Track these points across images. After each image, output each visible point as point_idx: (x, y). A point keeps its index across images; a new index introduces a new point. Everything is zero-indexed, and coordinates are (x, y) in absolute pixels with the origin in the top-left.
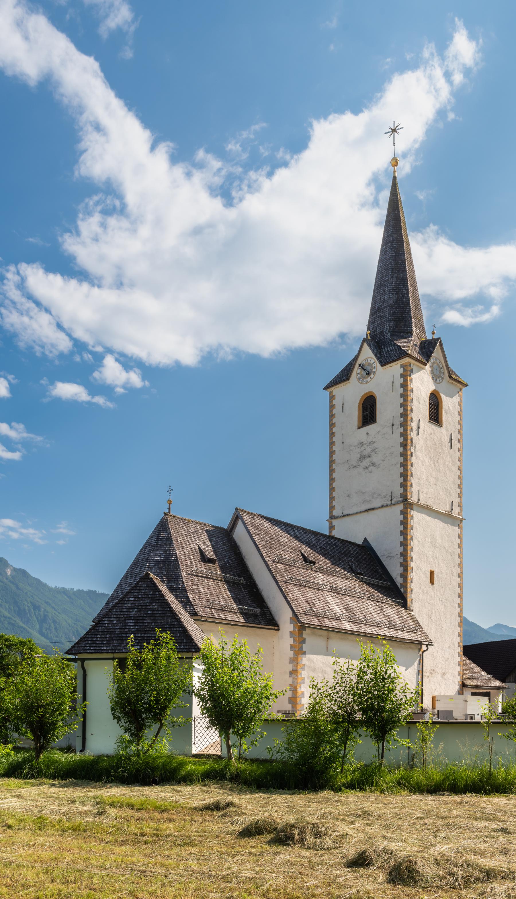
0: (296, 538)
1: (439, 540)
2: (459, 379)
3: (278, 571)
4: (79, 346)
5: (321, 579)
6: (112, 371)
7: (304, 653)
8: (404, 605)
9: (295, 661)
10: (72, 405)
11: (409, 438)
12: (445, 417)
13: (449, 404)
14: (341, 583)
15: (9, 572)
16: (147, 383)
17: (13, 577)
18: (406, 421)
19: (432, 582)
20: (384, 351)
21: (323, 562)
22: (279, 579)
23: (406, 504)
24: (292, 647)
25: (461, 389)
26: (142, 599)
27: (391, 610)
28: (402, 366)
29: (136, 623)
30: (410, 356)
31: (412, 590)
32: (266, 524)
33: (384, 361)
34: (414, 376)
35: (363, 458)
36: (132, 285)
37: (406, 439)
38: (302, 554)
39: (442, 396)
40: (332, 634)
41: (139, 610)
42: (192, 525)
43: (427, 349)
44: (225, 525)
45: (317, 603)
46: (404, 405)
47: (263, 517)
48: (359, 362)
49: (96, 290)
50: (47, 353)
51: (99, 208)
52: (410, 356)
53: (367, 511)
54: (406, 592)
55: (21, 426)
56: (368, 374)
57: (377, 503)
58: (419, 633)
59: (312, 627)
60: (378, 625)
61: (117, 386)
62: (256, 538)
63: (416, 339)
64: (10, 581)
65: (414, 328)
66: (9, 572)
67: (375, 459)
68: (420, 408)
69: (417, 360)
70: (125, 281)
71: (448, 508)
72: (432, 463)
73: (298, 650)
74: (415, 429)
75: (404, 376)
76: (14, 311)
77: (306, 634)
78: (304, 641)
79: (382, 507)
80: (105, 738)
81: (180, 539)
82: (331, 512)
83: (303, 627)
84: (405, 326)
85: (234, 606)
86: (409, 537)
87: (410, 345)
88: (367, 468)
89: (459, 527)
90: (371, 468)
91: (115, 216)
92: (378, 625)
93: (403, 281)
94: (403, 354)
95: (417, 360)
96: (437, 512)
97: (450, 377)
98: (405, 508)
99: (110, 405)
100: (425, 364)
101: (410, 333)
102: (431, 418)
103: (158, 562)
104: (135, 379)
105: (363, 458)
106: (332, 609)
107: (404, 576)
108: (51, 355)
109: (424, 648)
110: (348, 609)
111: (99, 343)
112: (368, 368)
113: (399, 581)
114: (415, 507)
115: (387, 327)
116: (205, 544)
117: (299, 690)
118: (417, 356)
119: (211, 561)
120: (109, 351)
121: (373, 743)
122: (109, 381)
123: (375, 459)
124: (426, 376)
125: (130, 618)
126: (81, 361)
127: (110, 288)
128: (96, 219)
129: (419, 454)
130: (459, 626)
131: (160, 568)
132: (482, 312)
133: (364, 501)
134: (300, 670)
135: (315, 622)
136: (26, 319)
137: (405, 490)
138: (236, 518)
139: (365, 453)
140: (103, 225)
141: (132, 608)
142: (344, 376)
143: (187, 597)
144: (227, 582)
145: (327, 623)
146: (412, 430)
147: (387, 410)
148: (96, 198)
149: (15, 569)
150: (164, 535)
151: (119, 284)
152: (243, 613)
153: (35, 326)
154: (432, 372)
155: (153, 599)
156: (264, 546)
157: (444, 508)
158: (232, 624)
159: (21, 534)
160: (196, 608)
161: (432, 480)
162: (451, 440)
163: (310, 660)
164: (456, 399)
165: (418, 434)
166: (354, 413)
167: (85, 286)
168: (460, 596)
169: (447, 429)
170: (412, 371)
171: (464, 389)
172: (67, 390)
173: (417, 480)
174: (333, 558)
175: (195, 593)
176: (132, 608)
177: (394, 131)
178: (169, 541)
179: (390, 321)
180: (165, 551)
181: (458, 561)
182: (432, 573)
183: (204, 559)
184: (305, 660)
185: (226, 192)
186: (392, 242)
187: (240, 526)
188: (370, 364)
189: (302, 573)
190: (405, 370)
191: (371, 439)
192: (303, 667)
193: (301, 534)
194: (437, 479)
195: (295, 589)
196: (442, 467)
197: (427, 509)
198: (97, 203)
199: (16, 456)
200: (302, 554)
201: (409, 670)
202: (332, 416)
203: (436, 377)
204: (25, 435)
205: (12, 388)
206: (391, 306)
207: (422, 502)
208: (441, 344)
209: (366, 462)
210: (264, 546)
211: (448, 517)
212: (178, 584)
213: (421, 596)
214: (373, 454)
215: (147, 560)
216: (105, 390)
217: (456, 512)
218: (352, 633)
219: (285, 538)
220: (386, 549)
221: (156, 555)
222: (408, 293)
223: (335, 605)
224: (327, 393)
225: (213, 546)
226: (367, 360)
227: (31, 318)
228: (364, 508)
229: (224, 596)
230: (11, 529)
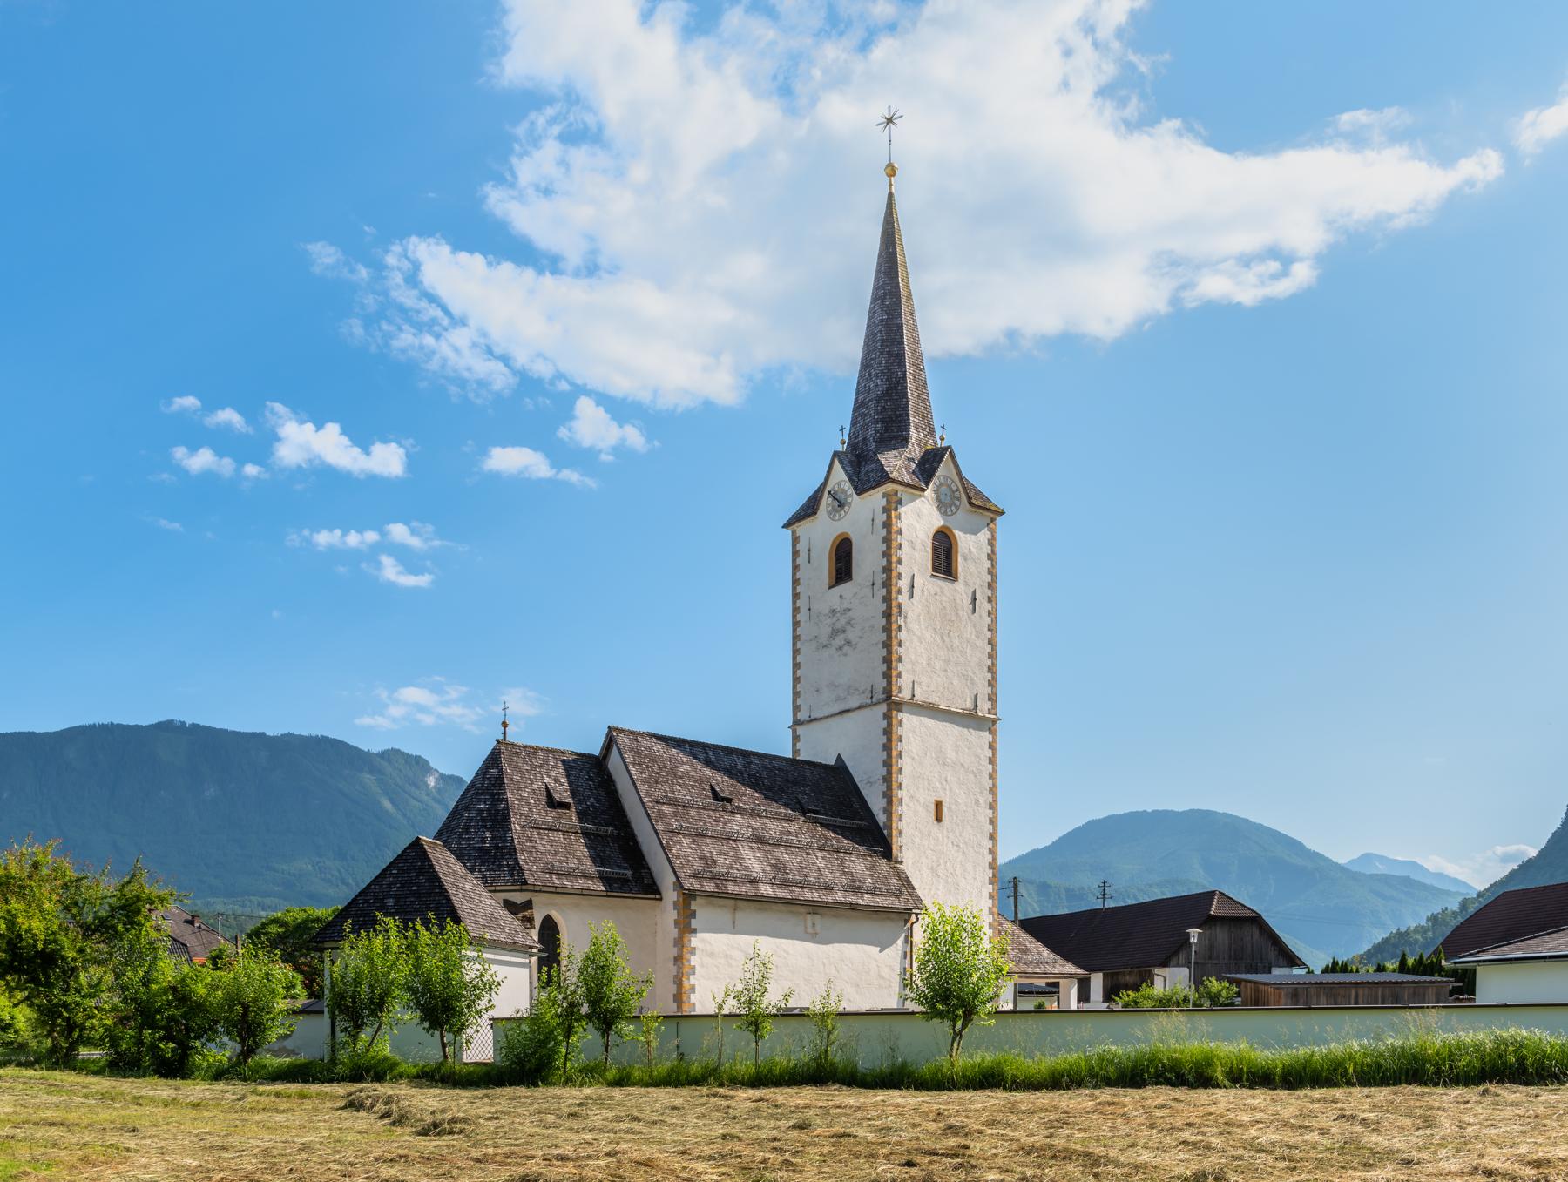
0: (708, 763)
1: (951, 755)
2: (988, 505)
3: (660, 815)
4: (527, 383)
5: (737, 823)
6: (591, 426)
7: (694, 931)
8: (887, 854)
9: (680, 943)
10: (520, 484)
11: (894, 604)
12: (961, 565)
13: (970, 545)
14: (773, 828)
15: (431, 781)
16: (656, 443)
17: (439, 790)
18: (889, 578)
19: (938, 818)
20: (863, 471)
21: (748, 797)
22: (660, 826)
23: (890, 703)
24: (676, 923)
25: (993, 520)
26: (408, 871)
27: (860, 865)
28: (885, 495)
29: (396, 903)
30: (895, 481)
31: (900, 833)
32: (658, 747)
33: (861, 488)
34: (902, 510)
35: (835, 632)
36: (614, 270)
37: (889, 607)
38: (712, 788)
39: (957, 533)
40: (741, 903)
41: (403, 886)
42: (540, 755)
43: (928, 465)
44: (596, 751)
45: (720, 860)
46: (887, 555)
47: (652, 735)
48: (829, 487)
49: (548, 280)
50: (471, 395)
51: (556, 130)
52: (895, 481)
53: (840, 713)
54: (890, 835)
55: (430, 528)
56: (841, 505)
57: (854, 702)
58: (905, 895)
59: (706, 895)
60: (828, 888)
61: (600, 451)
62: (633, 770)
63: (914, 450)
64: (434, 799)
65: (913, 432)
66: (431, 781)
67: (852, 635)
68: (915, 556)
69: (907, 485)
70: (602, 261)
71: (969, 704)
72: (938, 638)
73: (685, 927)
74: (905, 589)
75: (887, 510)
76: (406, 327)
77: (694, 905)
78: (693, 914)
79: (860, 708)
80: (312, 1037)
81: (516, 778)
82: (795, 715)
83: (690, 896)
84: (899, 429)
85: (589, 866)
86: (894, 753)
87: (896, 462)
88: (840, 648)
89: (992, 732)
90: (846, 648)
91: (584, 148)
92: (828, 888)
93: (900, 358)
94: (884, 478)
95: (907, 485)
96: (949, 712)
97: (971, 504)
98: (889, 710)
99: (591, 483)
100: (923, 490)
101: (906, 440)
102: (935, 569)
103: (480, 811)
104: (634, 437)
105: (835, 632)
106: (746, 868)
107: (888, 811)
108: (479, 401)
109: (913, 918)
110: (777, 866)
111: (560, 376)
112: (841, 497)
113: (882, 819)
114: (905, 708)
115: (871, 432)
116: (556, 781)
117: (685, 983)
118: (907, 478)
119: (565, 806)
120: (580, 390)
121: (598, 1035)
122: (586, 443)
123: (852, 635)
124: (927, 506)
125: (390, 896)
126: (536, 405)
127: (577, 274)
128: (551, 150)
129: (914, 626)
130: (991, 882)
131: (483, 820)
132: (1275, 277)
133: (838, 699)
134: (686, 956)
135: (710, 886)
136: (429, 340)
137: (889, 683)
138: (610, 742)
139: (838, 626)
140: (563, 163)
141: (394, 883)
142: (809, 509)
143: (516, 860)
144: (585, 834)
145: (731, 888)
146: (899, 592)
147: (866, 562)
148: (550, 111)
149: (443, 777)
150: (494, 772)
151: (591, 269)
152: (604, 878)
153: (445, 349)
154: (938, 499)
155: (420, 872)
156: (646, 781)
157: (961, 704)
158: (583, 893)
159: (439, 716)
160: (527, 874)
161: (938, 664)
162: (974, 599)
163: (703, 941)
164: (984, 535)
165: (912, 596)
166: (823, 565)
167: (529, 274)
168: (992, 837)
169: (966, 584)
170: (900, 502)
171: (999, 520)
172: (508, 459)
173: (909, 666)
174: (770, 789)
175: (530, 853)
176: (394, 883)
177: (890, 121)
178: (499, 781)
179: (877, 422)
180: (492, 796)
181: (988, 783)
182: (938, 805)
183: (552, 803)
184: (695, 941)
185: (785, 87)
186: (883, 299)
187: (614, 752)
188: (844, 491)
189: (705, 819)
190: (888, 502)
191: (845, 606)
192: (693, 951)
193: (717, 756)
194: (947, 661)
195: (686, 842)
196: (957, 642)
197: (928, 709)
198: (552, 121)
199: (423, 580)
200: (712, 788)
201: (887, 951)
202: (795, 568)
203: (943, 506)
204: (437, 543)
205: (411, 462)
206: (878, 399)
207: (919, 698)
208: (952, 455)
209: (839, 640)
210: (646, 781)
211: (969, 719)
212: (505, 841)
213: (917, 840)
214: (848, 628)
215: (467, 809)
216: (583, 458)
217: (984, 708)
218: (776, 901)
219: (687, 764)
220: (865, 773)
221: (479, 802)
222: (904, 378)
223: (754, 862)
224: (788, 533)
225: (570, 784)
226: (839, 484)
227: (438, 337)
228: (836, 709)
229: (579, 854)
230: (421, 708)
